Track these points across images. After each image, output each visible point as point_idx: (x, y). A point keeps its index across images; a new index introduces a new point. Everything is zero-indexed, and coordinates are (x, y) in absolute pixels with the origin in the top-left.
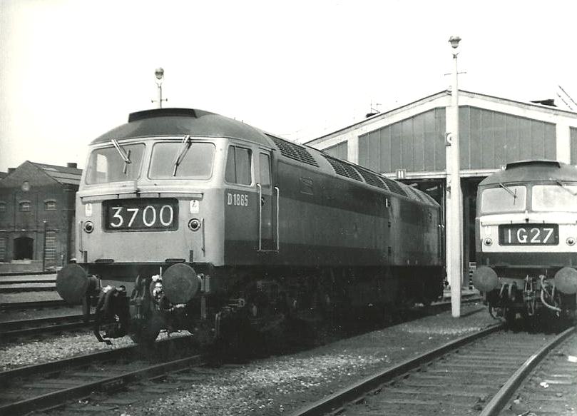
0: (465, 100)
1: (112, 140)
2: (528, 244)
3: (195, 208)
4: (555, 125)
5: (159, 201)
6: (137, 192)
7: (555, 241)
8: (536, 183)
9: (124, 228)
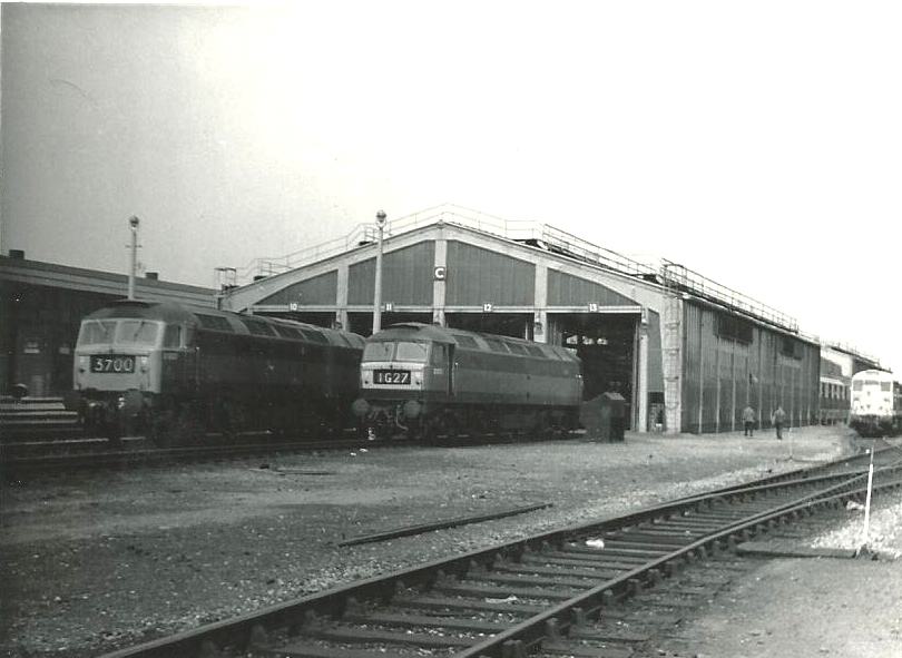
0: (452, 235)
1: (142, 635)
2: (392, 383)
3: (144, 361)
4: (534, 265)
5: (124, 356)
6: (111, 351)
7: (408, 382)
8: (402, 341)
9: (103, 372)
